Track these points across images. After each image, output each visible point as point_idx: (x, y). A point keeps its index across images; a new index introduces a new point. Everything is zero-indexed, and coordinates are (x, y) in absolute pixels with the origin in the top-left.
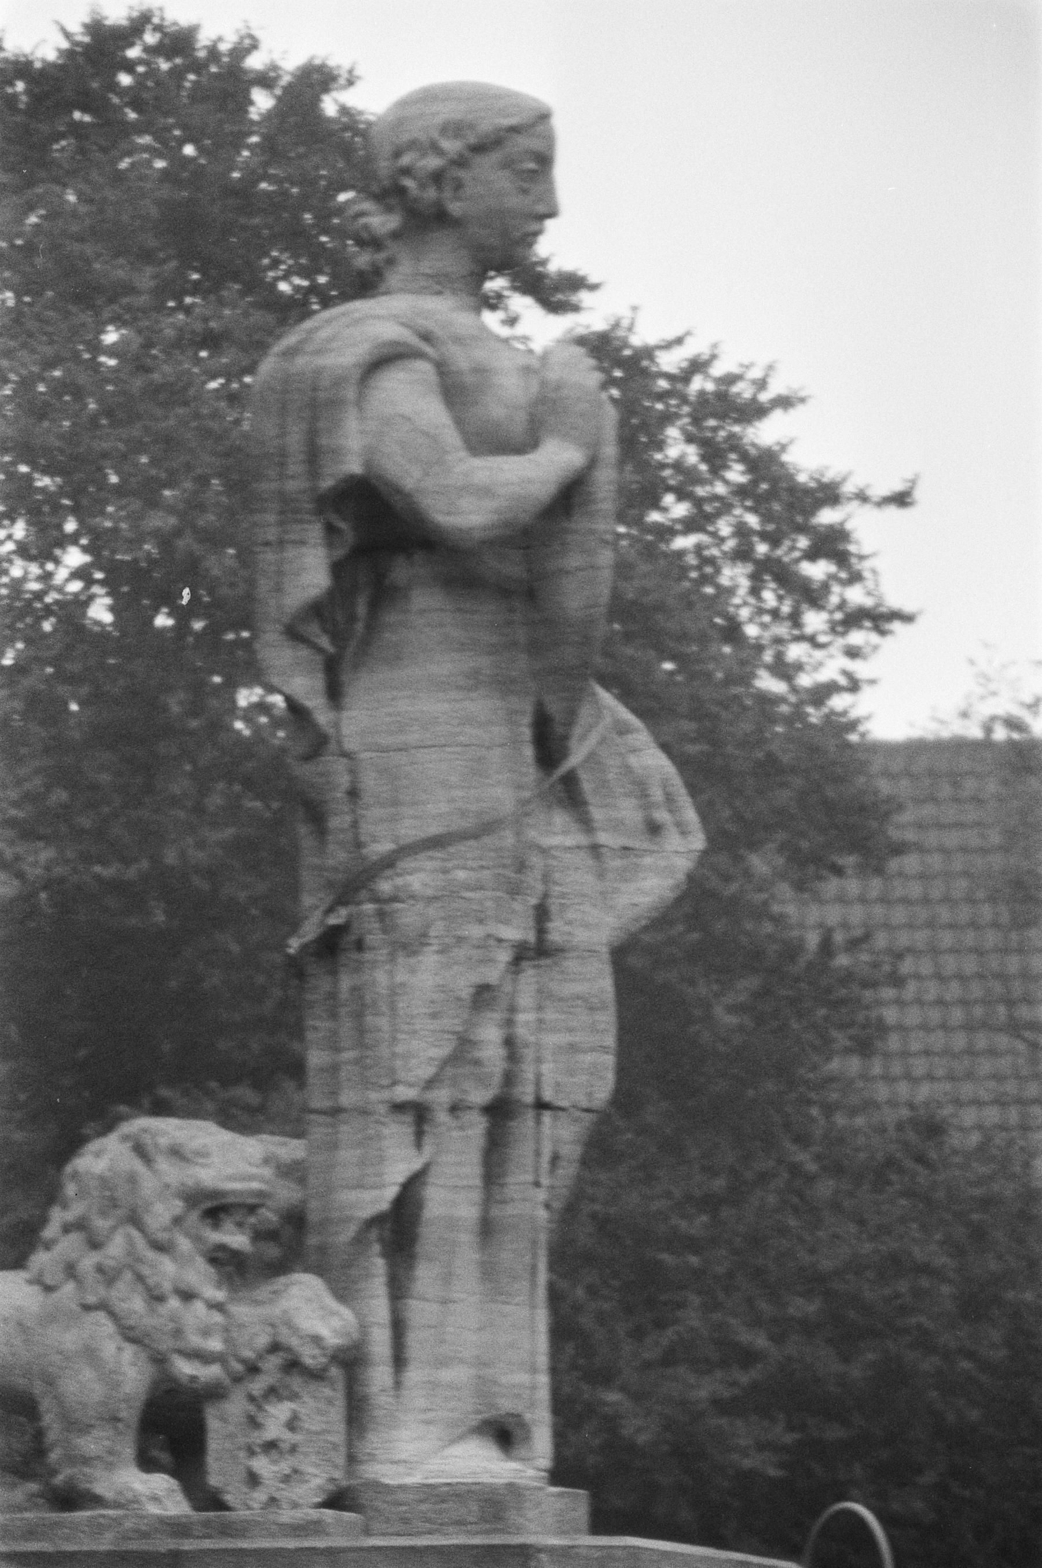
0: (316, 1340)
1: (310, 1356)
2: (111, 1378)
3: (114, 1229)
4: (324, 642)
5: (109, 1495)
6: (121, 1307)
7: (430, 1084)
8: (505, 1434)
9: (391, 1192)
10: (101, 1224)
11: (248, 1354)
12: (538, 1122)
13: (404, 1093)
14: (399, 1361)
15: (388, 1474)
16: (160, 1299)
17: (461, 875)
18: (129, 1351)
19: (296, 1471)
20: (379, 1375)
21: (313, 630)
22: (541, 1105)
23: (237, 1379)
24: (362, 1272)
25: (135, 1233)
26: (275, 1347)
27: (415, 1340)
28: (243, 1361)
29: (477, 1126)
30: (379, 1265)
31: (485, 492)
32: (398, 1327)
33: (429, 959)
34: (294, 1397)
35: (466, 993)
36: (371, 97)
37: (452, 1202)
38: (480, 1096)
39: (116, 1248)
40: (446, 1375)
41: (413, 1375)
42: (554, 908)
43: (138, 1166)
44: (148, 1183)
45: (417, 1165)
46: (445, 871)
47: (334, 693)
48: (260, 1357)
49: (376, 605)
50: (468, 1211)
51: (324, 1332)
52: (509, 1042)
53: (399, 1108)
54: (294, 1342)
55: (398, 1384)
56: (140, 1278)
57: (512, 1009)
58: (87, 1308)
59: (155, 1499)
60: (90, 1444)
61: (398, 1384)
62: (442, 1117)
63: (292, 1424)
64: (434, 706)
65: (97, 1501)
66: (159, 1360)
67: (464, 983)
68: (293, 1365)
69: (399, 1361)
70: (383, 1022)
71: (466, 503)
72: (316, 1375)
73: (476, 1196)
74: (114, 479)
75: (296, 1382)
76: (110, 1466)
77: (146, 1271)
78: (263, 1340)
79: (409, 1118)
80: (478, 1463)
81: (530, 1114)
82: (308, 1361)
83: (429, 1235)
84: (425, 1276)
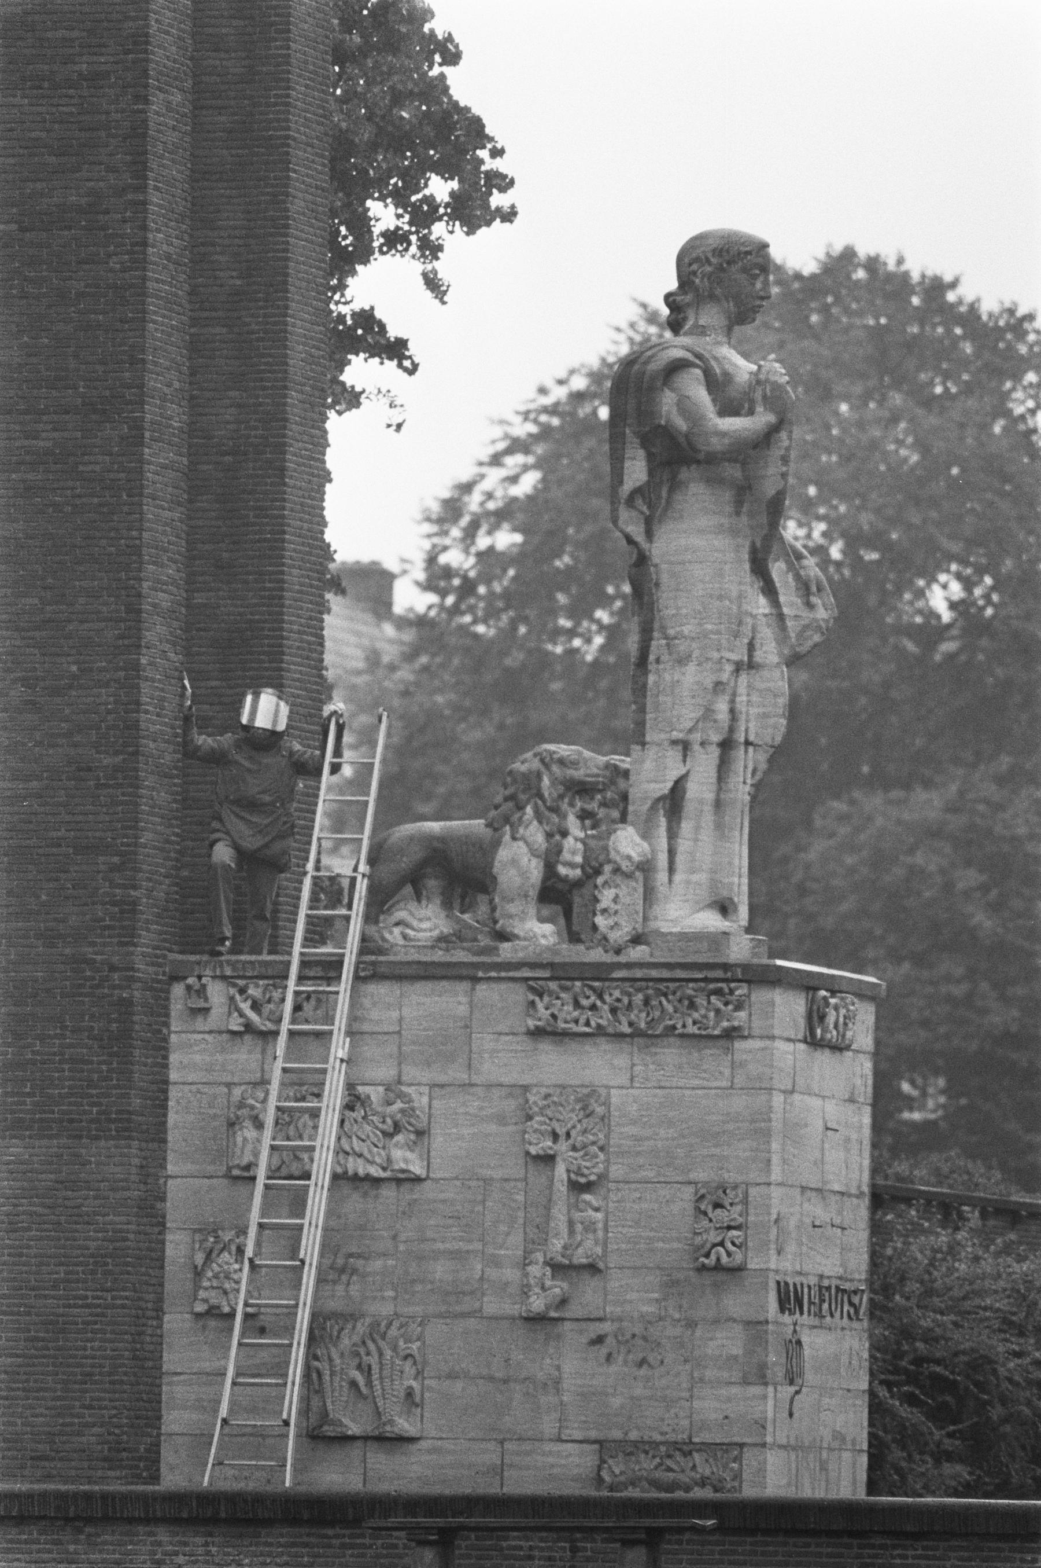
0: (629, 858)
1: (625, 865)
2: (524, 874)
4: (645, 509)
5: (522, 934)
6: (530, 840)
7: (690, 731)
8: (725, 908)
9: (670, 785)
10: (522, 797)
12: (746, 752)
13: (675, 735)
14: (671, 870)
15: (665, 928)
17: (709, 627)
20: (662, 876)
21: (639, 502)
22: (748, 743)
25: (540, 802)
27: (680, 859)
29: (715, 752)
30: (663, 821)
31: (724, 434)
32: (672, 853)
33: (691, 668)
34: (617, 886)
35: (710, 686)
37: (700, 789)
38: (716, 738)
40: (695, 878)
41: (678, 877)
42: (757, 646)
43: (543, 769)
45: (683, 771)
47: (649, 534)
49: (671, 490)
50: (710, 796)
51: (633, 854)
52: (732, 711)
53: (674, 742)
55: (670, 881)
57: (734, 695)
59: (544, 936)
60: (512, 908)
61: (670, 881)
62: (696, 747)
63: (616, 900)
64: (697, 541)
65: (517, 937)
67: (709, 682)
68: (617, 870)
69: (671, 870)
71: (714, 440)
72: (629, 876)
73: (714, 788)
75: (618, 879)
76: (522, 920)
79: (680, 748)
80: (711, 921)
81: (742, 748)
83: (689, 807)
84: (686, 827)
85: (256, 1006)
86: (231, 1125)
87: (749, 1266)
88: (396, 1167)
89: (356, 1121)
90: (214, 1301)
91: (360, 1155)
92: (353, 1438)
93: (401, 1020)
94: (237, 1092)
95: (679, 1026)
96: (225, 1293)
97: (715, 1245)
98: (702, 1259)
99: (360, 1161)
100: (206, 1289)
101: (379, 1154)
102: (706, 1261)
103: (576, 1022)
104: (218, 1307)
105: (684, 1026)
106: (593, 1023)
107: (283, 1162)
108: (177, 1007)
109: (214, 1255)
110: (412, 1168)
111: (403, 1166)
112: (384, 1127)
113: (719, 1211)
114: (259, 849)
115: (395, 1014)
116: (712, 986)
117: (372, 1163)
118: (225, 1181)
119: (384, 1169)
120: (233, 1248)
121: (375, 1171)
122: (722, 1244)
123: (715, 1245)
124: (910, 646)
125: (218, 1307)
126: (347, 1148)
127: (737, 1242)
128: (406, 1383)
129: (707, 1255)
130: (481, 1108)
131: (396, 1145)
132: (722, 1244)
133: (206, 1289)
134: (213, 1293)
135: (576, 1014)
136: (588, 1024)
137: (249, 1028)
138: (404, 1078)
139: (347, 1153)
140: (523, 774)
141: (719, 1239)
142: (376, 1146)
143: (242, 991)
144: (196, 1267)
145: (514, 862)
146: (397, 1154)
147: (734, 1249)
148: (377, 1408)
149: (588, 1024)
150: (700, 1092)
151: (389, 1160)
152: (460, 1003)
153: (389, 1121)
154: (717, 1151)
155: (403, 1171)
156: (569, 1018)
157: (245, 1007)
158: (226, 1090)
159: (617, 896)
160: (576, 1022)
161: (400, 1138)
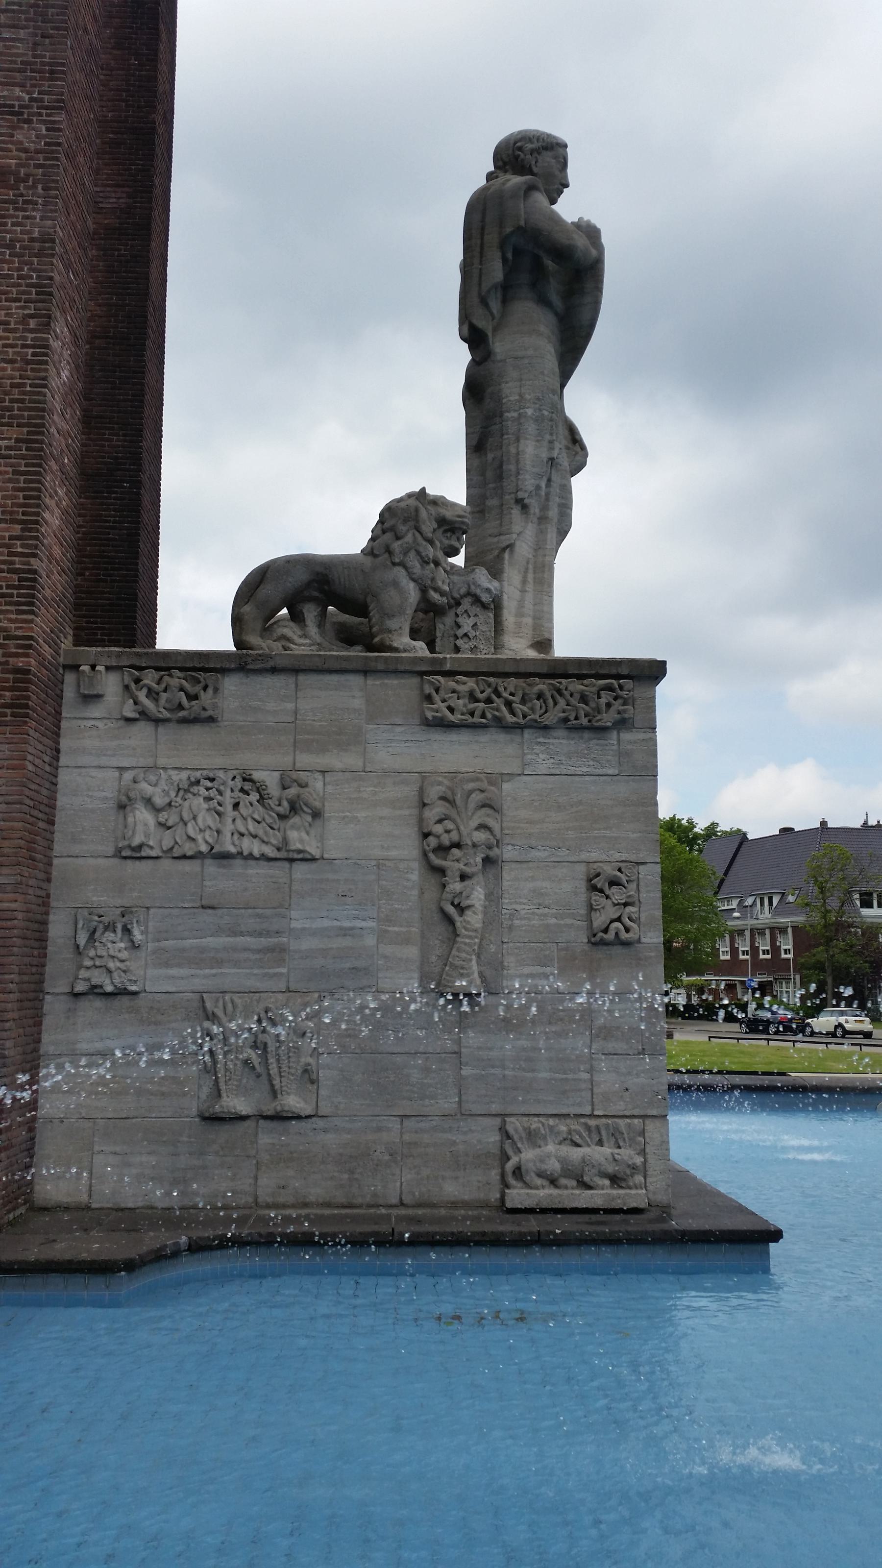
0: (488, 590)
3: (408, 530)
10: (402, 528)
11: (457, 596)
16: (428, 563)
18: (412, 585)
19: (475, 646)
23: (450, 607)
24: (228, 799)
25: (417, 534)
26: (469, 594)
28: (453, 598)
36: (577, 482)
39: (409, 538)
44: (423, 514)
46: (540, 410)
48: (462, 597)
54: (478, 592)
56: (418, 553)
58: (394, 564)
66: (424, 590)
70: (512, 467)
74: (869, 1005)
77: (421, 549)
78: (463, 591)
82: (484, 599)
85: (152, 694)
86: (122, 807)
87: (643, 940)
88: (293, 848)
89: (251, 804)
90: (95, 981)
91: (255, 837)
92: (243, 1118)
93: (296, 712)
94: (128, 776)
95: (572, 718)
96: (109, 971)
97: (612, 921)
98: (601, 934)
99: (256, 842)
100: (88, 968)
101: (275, 835)
102: (605, 936)
103: (472, 714)
104: (101, 987)
105: (576, 718)
106: (489, 716)
107: (176, 843)
108: (69, 693)
109: (97, 934)
110: (308, 849)
111: (299, 846)
112: (280, 809)
113: (614, 889)
114: (556, 314)
115: (290, 706)
116: (602, 682)
117: (266, 843)
118: (116, 861)
119: (279, 849)
120: (119, 927)
121: (270, 851)
122: (619, 919)
123: (612, 921)
124: (490, 557)
125: (101, 987)
126: (242, 829)
127: (634, 916)
128: (303, 1060)
129: (606, 931)
130: (375, 793)
131: (293, 827)
132: (619, 919)
133: (88, 968)
134: (96, 972)
135: (472, 706)
136: (483, 716)
137: (144, 715)
138: (298, 766)
139: (242, 835)
140: (402, 509)
141: (616, 916)
142: (272, 828)
143: (137, 681)
144: (78, 947)
145: (395, 584)
146: (293, 835)
147: (632, 924)
148: (272, 1086)
149: (483, 716)
150: (587, 778)
151: (285, 841)
152: (354, 697)
153: (285, 804)
154: (608, 833)
155: (300, 851)
156: (465, 710)
157: (142, 695)
158: (117, 774)
159: (476, 624)
160: (472, 714)
161: (296, 820)
